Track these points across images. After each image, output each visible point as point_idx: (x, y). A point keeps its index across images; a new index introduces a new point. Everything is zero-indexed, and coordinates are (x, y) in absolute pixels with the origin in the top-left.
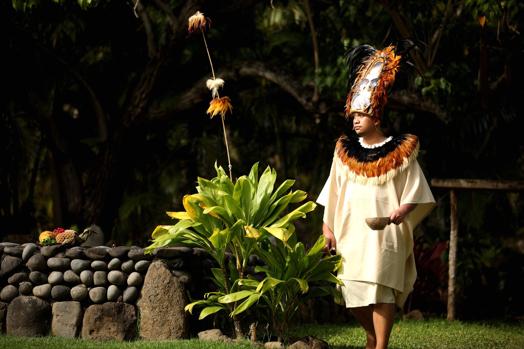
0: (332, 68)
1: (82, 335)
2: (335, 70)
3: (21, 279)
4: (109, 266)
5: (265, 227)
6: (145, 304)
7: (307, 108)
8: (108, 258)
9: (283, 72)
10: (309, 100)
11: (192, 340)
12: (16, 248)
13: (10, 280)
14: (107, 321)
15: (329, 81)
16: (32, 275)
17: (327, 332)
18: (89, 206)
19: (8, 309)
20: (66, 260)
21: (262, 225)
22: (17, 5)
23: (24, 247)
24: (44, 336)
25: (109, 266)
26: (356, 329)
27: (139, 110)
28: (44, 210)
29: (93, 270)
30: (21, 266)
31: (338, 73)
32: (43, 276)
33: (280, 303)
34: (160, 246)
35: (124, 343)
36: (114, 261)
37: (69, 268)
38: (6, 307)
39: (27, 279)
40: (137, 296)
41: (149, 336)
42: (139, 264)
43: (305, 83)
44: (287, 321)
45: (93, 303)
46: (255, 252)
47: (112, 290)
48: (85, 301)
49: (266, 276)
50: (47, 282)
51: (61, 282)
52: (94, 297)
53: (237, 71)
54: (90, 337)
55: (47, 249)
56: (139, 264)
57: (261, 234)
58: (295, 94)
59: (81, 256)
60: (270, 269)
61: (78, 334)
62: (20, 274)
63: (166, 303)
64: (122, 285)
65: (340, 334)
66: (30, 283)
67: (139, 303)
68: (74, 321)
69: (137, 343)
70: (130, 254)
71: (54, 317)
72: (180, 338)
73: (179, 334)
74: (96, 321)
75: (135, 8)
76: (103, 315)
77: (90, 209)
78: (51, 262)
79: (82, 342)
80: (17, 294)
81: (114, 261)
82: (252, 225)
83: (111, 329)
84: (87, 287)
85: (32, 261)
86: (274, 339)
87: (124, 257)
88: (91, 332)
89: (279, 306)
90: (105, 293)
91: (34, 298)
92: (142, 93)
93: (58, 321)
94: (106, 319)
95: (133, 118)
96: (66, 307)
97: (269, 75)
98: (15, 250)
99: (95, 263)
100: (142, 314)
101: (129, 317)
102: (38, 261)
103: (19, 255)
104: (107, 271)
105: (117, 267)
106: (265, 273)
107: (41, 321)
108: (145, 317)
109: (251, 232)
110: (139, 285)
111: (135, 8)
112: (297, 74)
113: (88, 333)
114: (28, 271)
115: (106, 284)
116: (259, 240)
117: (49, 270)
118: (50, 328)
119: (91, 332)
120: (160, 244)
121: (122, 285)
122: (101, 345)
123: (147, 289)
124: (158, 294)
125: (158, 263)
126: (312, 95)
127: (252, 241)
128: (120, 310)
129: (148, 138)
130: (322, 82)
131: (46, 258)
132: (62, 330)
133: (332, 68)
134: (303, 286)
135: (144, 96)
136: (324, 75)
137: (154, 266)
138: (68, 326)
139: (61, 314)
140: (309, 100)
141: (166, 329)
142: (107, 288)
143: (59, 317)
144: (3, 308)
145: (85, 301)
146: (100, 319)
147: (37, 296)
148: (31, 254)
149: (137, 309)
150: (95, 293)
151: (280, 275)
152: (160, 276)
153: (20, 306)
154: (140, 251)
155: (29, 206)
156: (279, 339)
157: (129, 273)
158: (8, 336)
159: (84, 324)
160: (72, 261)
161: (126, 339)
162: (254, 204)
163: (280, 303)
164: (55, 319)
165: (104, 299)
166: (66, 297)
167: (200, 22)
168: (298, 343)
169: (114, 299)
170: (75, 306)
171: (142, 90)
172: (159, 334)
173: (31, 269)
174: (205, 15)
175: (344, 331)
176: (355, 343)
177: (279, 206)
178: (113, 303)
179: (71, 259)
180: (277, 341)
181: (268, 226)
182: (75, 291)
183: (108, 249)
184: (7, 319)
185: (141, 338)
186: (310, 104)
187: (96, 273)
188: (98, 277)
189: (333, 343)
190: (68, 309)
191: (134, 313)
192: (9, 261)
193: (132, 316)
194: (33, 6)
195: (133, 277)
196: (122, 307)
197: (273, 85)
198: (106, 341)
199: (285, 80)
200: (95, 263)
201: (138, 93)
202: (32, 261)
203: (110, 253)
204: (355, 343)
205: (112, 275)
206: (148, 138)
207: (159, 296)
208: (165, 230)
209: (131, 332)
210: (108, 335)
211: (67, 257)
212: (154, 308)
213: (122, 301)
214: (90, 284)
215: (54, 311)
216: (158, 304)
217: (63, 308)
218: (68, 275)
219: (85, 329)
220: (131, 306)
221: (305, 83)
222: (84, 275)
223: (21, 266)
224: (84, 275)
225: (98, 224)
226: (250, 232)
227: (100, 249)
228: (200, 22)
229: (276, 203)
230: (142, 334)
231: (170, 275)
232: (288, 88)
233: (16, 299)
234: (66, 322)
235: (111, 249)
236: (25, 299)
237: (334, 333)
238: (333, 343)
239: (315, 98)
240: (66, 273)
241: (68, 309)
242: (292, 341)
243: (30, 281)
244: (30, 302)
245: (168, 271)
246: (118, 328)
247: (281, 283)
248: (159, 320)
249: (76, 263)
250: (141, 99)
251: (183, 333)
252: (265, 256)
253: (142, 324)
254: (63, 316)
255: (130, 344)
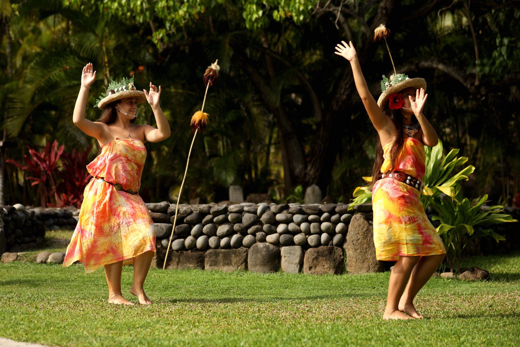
0: (489, 60)
1: (304, 271)
2: (491, 61)
3: (257, 230)
4: (322, 219)
5: (437, 186)
6: (349, 247)
7: (471, 91)
8: (320, 213)
9: (452, 64)
10: (472, 84)
11: (385, 273)
12: (253, 207)
13: (249, 231)
14: (322, 260)
15: (487, 69)
16: (265, 227)
17: (490, 262)
18: (310, 170)
19: (249, 253)
20: (289, 215)
21: (435, 185)
22: (250, 25)
23: (258, 206)
24: (276, 272)
25: (322, 219)
26: (512, 259)
27: (345, 97)
28: (278, 174)
29: (310, 222)
30: (257, 221)
31: (493, 63)
32: (273, 227)
33: (452, 244)
34: (359, 204)
35: (335, 276)
36: (325, 215)
37: (292, 221)
38: (247, 251)
39: (261, 230)
40: (343, 241)
41: (354, 270)
42: (343, 217)
43: (468, 72)
44: (457, 256)
45: (310, 247)
46: (431, 205)
47: (324, 236)
48: (305, 246)
49: (440, 223)
50: (276, 232)
51: (286, 232)
52: (311, 242)
53: (417, 65)
54: (310, 272)
55: (275, 208)
56: (343, 217)
57: (435, 191)
58: (461, 80)
59: (300, 212)
60: (443, 218)
61: (300, 270)
62: (256, 226)
63: (365, 246)
64: (332, 233)
65: (499, 263)
66: (264, 233)
67: (345, 246)
68: (297, 260)
69: (345, 276)
70: (337, 210)
71: (283, 258)
72: (377, 271)
73: (376, 269)
74: (313, 260)
75: (336, 22)
76: (318, 255)
77: (311, 173)
78: (279, 217)
79: (304, 276)
80: (255, 242)
81: (325, 215)
82: (427, 185)
83: (325, 266)
84: (306, 235)
85: (264, 217)
86: (448, 270)
87: (332, 212)
88: (310, 268)
89: (451, 245)
90: (319, 240)
91: (267, 244)
92: (346, 85)
93: (286, 261)
94: (320, 258)
95: (340, 103)
96: (291, 250)
97: (441, 67)
98: (251, 209)
99: (311, 217)
100: (348, 254)
101: (338, 256)
102: (269, 217)
103: (255, 212)
104: (320, 222)
105: (328, 220)
106: (439, 221)
107: (273, 262)
108: (350, 256)
109: (427, 191)
110: (344, 232)
111: (336, 22)
112: (462, 66)
113: (308, 269)
114: (262, 224)
115: (320, 233)
116: (433, 196)
117: (277, 223)
118: (280, 266)
119: (310, 268)
120: (359, 202)
121: (332, 233)
122: (317, 278)
123: (350, 236)
124: (359, 239)
125: (358, 215)
126: (475, 81)
127: (428, 197)
128: (331, 251)
129: (352, 117)
130: (481, 71)
131: (275, 214)
132: (289, 267)
133: (489, 60)
134: (470, 230)
135: (348, 86)
136: (483, 65)
137: (355, 218)
138: (293, 265)
139: (287, 256)
140: (472, 84)
141: (366, 265)
142: (320, 235)
143: (286, 258)
144: (245, 252)
145: (305, 246)
146: (316, 258)
147: (270, 243)
148: (263, 211)
149: (343, 251)
150: (312, 240)
151: (450, 222)
152: (360, 225)
153: (257, 251)
154: (344, 207)
155: (266, 172)
156: (451, 270)
157: (337, 224)
158: (249, 272)
159: (305, 263)
160: (294, 216)
161: (336, 273)
162: (429, 169)
163: (452, 244)
164: (283, 260)
165: (319, 244)
166: (290, 243)
167: (383, 32)
168: (466, 273)
169: (326, 243)
170: (297, 249)
171: (346, 82)
172: (361, 269)
173: (264, 222)
174: (387, 27)
175: (503, 260)
176: (510, 270)
177: (448, 169)
178: (326, 247)
179: (293, 214)
180: (450, 272)
181: (440, 185)
182: (297, 238)
183: (321, 206)
184: (248, 260)
185: (347, 272)
186: (473, 88)
187: (312, 224)
188: (314, 227)
189: (493, 271)
190: (292, 252)
191: (341, 254)
192: (248, 217)
193: (340, 256)
194: (261, 26)
195: (339, 227)
196: (333, 250)
197: (445, 75)
198: (321, 275)
199: (454, 70)
200: (311, 217)
201: (343, 85)
202: (264, 217)
203: (322, 209)
204: (510, 270)
205: (324, 225)
206: (352, 117)
207: (360, 241)
208: (362, 190)
209: (340, 268)
210: (323, 271)
211: (290, 213)
212: (356, 250)
213: (332, 245)
214: (308, 233)
215: (282, 253)
216: (359, 247)
217: (289, 251)
218: (291, 227)
219: (306, 266)
220: (339, 248)
221: (468, 72)
222: (303, 226)
223: (257, 221)
224: (303, 226)
225: (317, 184)
226: (426, 191)
227: (315, 207)
228: (383, 32)
229: (445, 168)
230: (348, 269)
231: (368, 224)
232: (456, 76)
233: (254, 245)
234: (292, 262)
235: (323, 206)
236: (261, 245)
237: (495, 263)
238: (493, 271)
239: (477, 83)
240: (290, 225)
241: (292, 252)
242: (462, 271)
243: (264, 231)
244: (264, 247)
245: (366, 222)
246: (330, 265)
247: (452, 229)
248: (360, 258)
249: (297, 218)
250: (345, 88)
251: (379, 268)
252: (439, 208)
253: (347, 261)
254: (289, 257)
255: (339, 277)
